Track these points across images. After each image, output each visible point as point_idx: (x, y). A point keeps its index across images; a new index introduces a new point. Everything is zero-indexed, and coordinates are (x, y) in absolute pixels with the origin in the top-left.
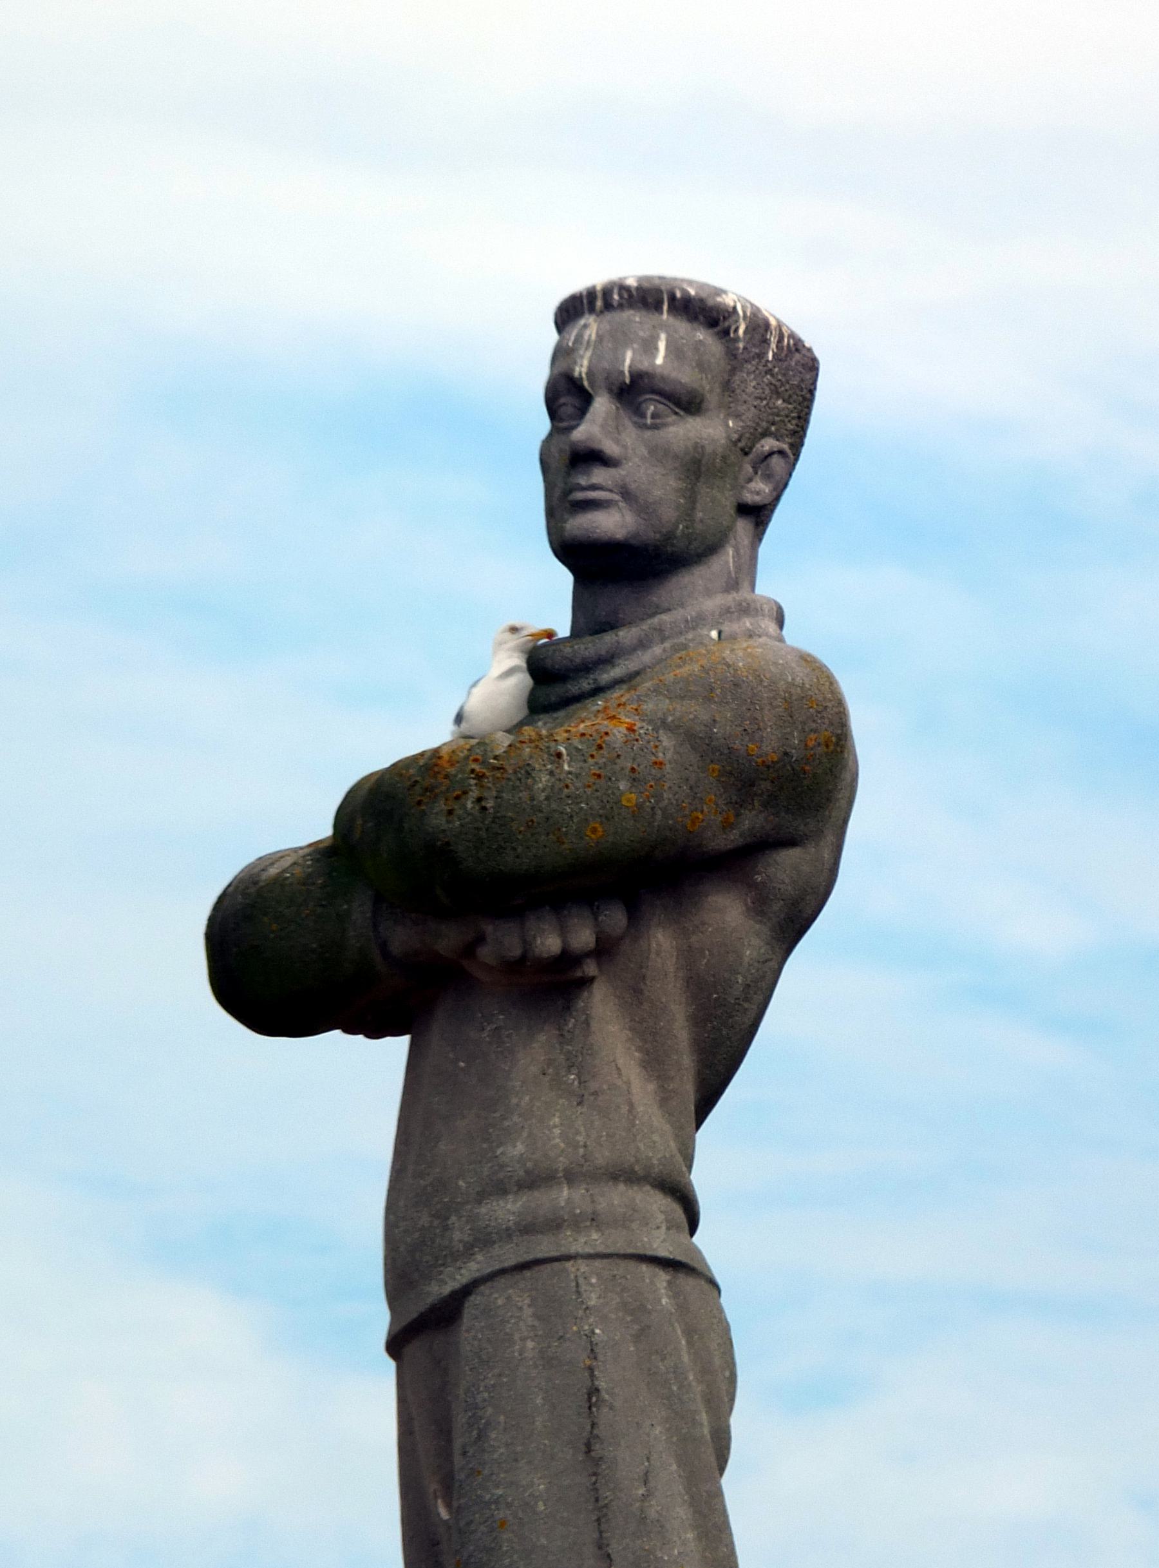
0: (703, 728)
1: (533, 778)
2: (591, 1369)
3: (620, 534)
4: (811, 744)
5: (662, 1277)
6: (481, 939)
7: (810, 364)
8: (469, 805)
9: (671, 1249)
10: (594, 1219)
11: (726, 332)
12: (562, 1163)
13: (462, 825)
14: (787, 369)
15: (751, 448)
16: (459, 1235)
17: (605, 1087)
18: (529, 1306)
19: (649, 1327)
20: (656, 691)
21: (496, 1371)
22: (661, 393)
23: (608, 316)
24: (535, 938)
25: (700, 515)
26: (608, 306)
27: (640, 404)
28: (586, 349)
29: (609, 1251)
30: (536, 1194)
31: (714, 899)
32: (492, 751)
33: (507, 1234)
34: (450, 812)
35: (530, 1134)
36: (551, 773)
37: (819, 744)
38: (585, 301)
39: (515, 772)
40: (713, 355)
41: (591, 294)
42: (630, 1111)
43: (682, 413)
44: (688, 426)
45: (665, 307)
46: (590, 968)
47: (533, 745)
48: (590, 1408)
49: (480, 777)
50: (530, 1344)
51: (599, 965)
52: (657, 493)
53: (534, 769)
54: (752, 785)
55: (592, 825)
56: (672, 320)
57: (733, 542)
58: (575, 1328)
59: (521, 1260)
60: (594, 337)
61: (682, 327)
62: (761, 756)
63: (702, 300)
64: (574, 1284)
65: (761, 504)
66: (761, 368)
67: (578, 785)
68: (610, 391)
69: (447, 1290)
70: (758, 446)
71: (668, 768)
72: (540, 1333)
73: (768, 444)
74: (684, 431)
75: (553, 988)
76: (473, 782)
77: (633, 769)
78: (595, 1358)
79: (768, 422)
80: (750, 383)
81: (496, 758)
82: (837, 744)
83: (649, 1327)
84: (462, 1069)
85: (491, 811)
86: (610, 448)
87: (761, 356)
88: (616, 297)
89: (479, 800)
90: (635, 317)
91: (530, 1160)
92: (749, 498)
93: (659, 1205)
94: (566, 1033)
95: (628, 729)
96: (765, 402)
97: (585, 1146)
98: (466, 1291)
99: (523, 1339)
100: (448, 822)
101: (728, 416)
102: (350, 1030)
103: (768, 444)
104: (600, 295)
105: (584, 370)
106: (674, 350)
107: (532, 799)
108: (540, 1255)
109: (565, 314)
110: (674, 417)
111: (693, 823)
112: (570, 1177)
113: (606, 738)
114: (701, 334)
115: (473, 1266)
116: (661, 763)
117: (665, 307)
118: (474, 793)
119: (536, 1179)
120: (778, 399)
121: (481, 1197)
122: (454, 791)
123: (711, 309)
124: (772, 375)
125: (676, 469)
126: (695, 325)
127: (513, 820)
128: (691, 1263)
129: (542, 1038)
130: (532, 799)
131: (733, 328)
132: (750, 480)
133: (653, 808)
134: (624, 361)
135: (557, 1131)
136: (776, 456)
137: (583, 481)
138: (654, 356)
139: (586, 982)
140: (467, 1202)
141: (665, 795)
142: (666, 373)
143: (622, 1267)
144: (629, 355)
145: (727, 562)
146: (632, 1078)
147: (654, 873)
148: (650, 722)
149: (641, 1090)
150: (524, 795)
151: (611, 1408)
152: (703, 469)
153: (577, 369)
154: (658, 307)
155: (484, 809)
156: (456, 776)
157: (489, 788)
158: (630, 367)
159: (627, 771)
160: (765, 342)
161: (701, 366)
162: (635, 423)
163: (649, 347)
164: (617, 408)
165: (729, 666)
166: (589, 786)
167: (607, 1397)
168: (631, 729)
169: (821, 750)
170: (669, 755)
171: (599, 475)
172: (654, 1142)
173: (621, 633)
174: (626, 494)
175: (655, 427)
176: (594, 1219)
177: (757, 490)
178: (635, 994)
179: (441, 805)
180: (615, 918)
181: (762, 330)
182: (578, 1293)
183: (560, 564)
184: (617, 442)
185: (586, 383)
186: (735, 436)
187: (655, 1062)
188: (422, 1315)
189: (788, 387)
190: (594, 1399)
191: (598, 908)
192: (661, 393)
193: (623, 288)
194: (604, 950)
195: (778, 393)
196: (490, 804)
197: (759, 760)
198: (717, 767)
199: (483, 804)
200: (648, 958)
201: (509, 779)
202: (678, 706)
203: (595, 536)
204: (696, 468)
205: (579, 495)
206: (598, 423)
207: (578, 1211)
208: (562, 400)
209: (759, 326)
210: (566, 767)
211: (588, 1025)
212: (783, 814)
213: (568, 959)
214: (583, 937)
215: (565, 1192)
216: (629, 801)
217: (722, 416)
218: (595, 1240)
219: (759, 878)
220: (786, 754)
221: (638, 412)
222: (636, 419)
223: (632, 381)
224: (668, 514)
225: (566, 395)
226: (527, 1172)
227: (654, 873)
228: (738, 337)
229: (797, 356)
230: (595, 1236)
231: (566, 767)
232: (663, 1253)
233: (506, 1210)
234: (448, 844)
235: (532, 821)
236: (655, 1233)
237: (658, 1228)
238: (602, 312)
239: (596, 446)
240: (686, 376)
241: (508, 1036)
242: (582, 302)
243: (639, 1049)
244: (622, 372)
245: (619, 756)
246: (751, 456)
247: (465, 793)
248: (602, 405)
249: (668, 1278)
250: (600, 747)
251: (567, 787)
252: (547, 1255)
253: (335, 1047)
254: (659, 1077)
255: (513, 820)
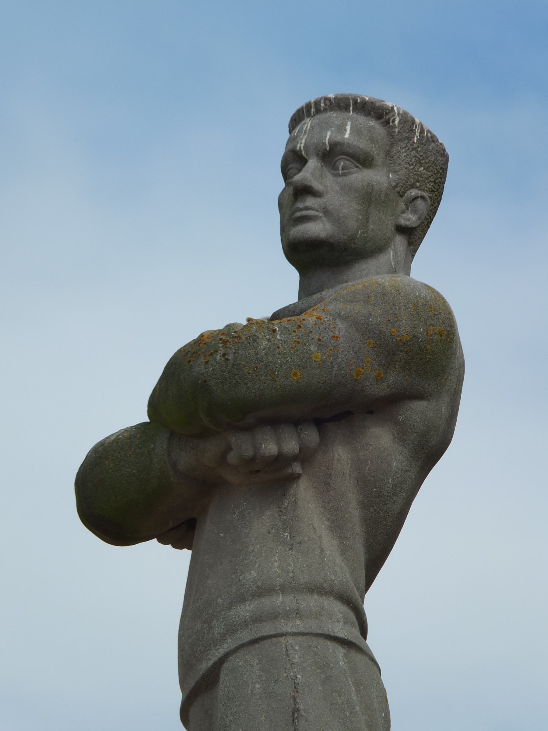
0: (363, 318)
1: (258, 343)
2: (294, 698)
3: (323, 235)
4: (431, 332)
5: (340, 651)
6: (229, 449)
7: (442, 152)
8: (218, 358)
9: (346, 634)
10: (298, 613)
11: (387, 122)
12: (279, 581)
13: (213, 370)
14: (426, 150)
15: (404, 193)
16: (218, 629)
17: (306, 539)
18: (258, 664)
19: (331, 677)
20: (336, 299)
21: (238, 703)
22: (347, 154)
23: (318, 116)
24: (261, 444)
25: (372, 227)
26: (318, 111)
27: (335, 163)
28: (305, 134)
29: (306, 631)
30: (263, 599)
31: (374, 430)
32: (233, 329)
33: (245, 624)
34: (207, 363)
35: (259, 566)
36: (269, 340)
37: (435, 333)
38: (305, 111)
39: (247, 339)
40: (380, 134)
41: (308, 106)
42: (321, 553)
43: (360, 167)
44: (364, 174)
45: (351, 108)
46: (297, 468)
47: (258, 325)
48: (293, 720)
49: (225, 342)
50: (258, 686)
51: (303, 468)
52: (345, 211)
53: (258, 338)
54: (394, 354)
55: (294, 371)
56: (355, 115)
57: (393, 247)
58: (285, 675)
59: (252, 638)
60: (309, 127)
61: (361, 119)
62: (399, 336)
63: (372, 103)
64: (284, 650)
65: (411, 226)
66: (409, 146)
67: (286, 347)
68: (318, 155)
69: (211, 663)
70: (408, 192)
71: (341, 340)
72: (264, 679)
73: (414, 192)
74: (361, 177)
75: (274, 479)
76: (221, 345)
77: (319, 339)
78: (297, 692)
79: (414, 179)
80: (402, 154)
81: (235, 332)
82: (448, 336)
83: (331, 677)
84: (221, 537)
85: (232, 361)
86: (316, 185)
87: (410, 139)
88: (322, 105)
89: (224, 355)
90: (334, 116)
91: (259, 580)
92: (402, 222)
93: (339, 609)
94: (282, 510)
95: (317, 318)
96: (412, 167)
97: (293, 572)
98: (222, 661)
99: (254, 683)
100: (205, 368)
101: (390, 171)
102: (163, 541)
103: (414, 192)
104: (313, 105)
105: (302, 145)
106: (355, 130)
107: (257, 354)
108: (264, 634)
109: (294, 122)
110: (356, 169)
111: (357, 375)
112: (284, 590)
113: (304, 322)
114: (372, 123)
115: (225, 646)
116: (337, 337)
117: (351, 108)
118: (222, 351)
119: (264, 591)
120: (421, 167)
121: (231, 606)
122: (210, 351)
123: (379, 108)
124: (417, 152)
125: (356, 197)
126: (369, 118)
127: (245, 366)
128: (359, 644)
129: (268, 513)
130: (257, 354)
131: (392, 119)
132: (404, 212)
133: (332, 363)
134: (326, 137)
135: (276, 564)
136: (419, 199)
137: (300, 205)
138: (344, 135)
139: (295, 478)
140: (223, 610)
141: (340, 356)
142: (350, 142)
143: (315, 641)
144: (329, 134)
145: (389, 258)
146: (323, 534)
147: (334, 409)
148: (331, 315)
149: (329, 544)
150: (252, 352)
151: (307, 720)
152: (373, 199)
153: (299, 145)
154: (347, 109)
155: (227, 359)
156: (211, 343)
157: (231, 348)
158: (329, 140)
159: (316, 340)
160: (412, 131)
161: (372, 140)
162: (332, 174)
163: (341, 129)
164: (322, 166)
165: (380, 285)
166: (292, 348)
167: (304, 714)
168: (319, 318)
169: (437, 337)
170: (341, 334)
171: (310, 201)
172: (336, 571)
173: (323, 293)
174: (326, 212)
175: (344, 175)
176: (298, 613)
177: (410, 219)
178: (325, 486)
179: (202, 360)
180: (311, 436)
181: (410, 124)
182: (287, 655)
183: (291, 265)
184: (321, 183)
185: (303, 153)
186: (394, 184)
187: (337, 527)
188: (197, 683)
189: (427, 161)
190: (296, 715)
191: (301, 430)
192: (347, 154)
193: (326, 99)
194: (305, 457)
195: (420, 163)
196: (231, 357)
197: (398, 339)
198: (372, 341)
199: (226, 357)
200: (332, 464)
201: (243, 343)
202: (348, 306)
203: (307, 236)
204: (368, 198)
205: (298, 214)
206: (310, 172)
207: (288, 608)
208: (290, 166)
209: (408, 122)
210: (278, 337)
211: (296, 503)
212: (414, 376)
213: (280, 461)
214: (291, 446)
215: (281, 598)
216: (316, 357)
217: (385, 170)
218: (298, 625)
219: (401, 418)
220: (414, 336)
221: (334, 167)
222: (333, 171)
223: (330, 148)
224: (352, 224)
225: (293, 161)
226: (257, 587)
227: (334, 409)
228: (395, 125)
229: (433, 145)
230: (298, 622)
231: (278, 337)
232: (341, 635)
233: (246, 610)
234: (205, 381)
235: (257, 367)
236: (337, 624)
237: (338, 621)
238: (314, 115)
239: (309, 184)
240: (363, 144)
241: (249, 513)
242: (303, 112)
243: (328, 519)
244: (325, 143)
245: (311, 332)
246: (404, 198)
247: (216, 351)
248: (313, 163)
249: (344, 651)
250: (299, 327)
251: (279, 348)
252: (268, 634)
253: (152, 549)
254: (340, 537)
255: (245, 366)
